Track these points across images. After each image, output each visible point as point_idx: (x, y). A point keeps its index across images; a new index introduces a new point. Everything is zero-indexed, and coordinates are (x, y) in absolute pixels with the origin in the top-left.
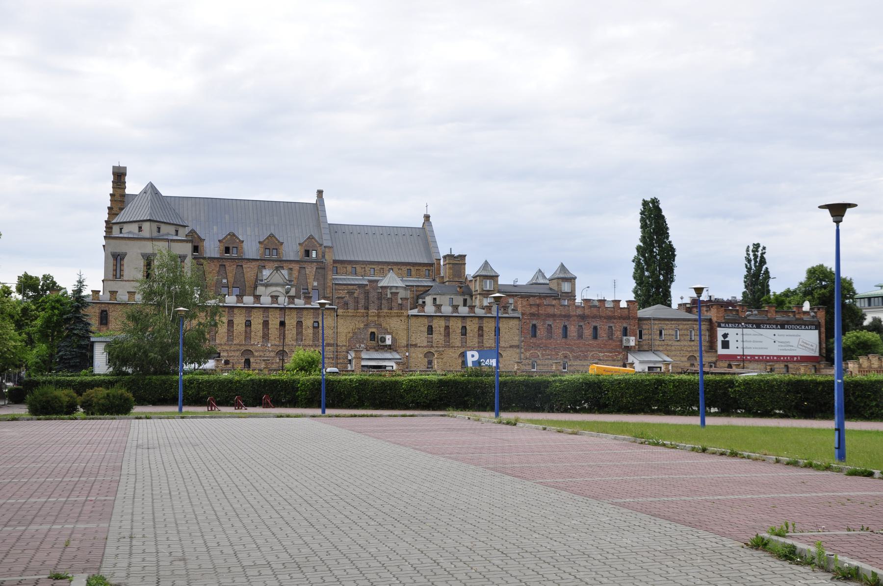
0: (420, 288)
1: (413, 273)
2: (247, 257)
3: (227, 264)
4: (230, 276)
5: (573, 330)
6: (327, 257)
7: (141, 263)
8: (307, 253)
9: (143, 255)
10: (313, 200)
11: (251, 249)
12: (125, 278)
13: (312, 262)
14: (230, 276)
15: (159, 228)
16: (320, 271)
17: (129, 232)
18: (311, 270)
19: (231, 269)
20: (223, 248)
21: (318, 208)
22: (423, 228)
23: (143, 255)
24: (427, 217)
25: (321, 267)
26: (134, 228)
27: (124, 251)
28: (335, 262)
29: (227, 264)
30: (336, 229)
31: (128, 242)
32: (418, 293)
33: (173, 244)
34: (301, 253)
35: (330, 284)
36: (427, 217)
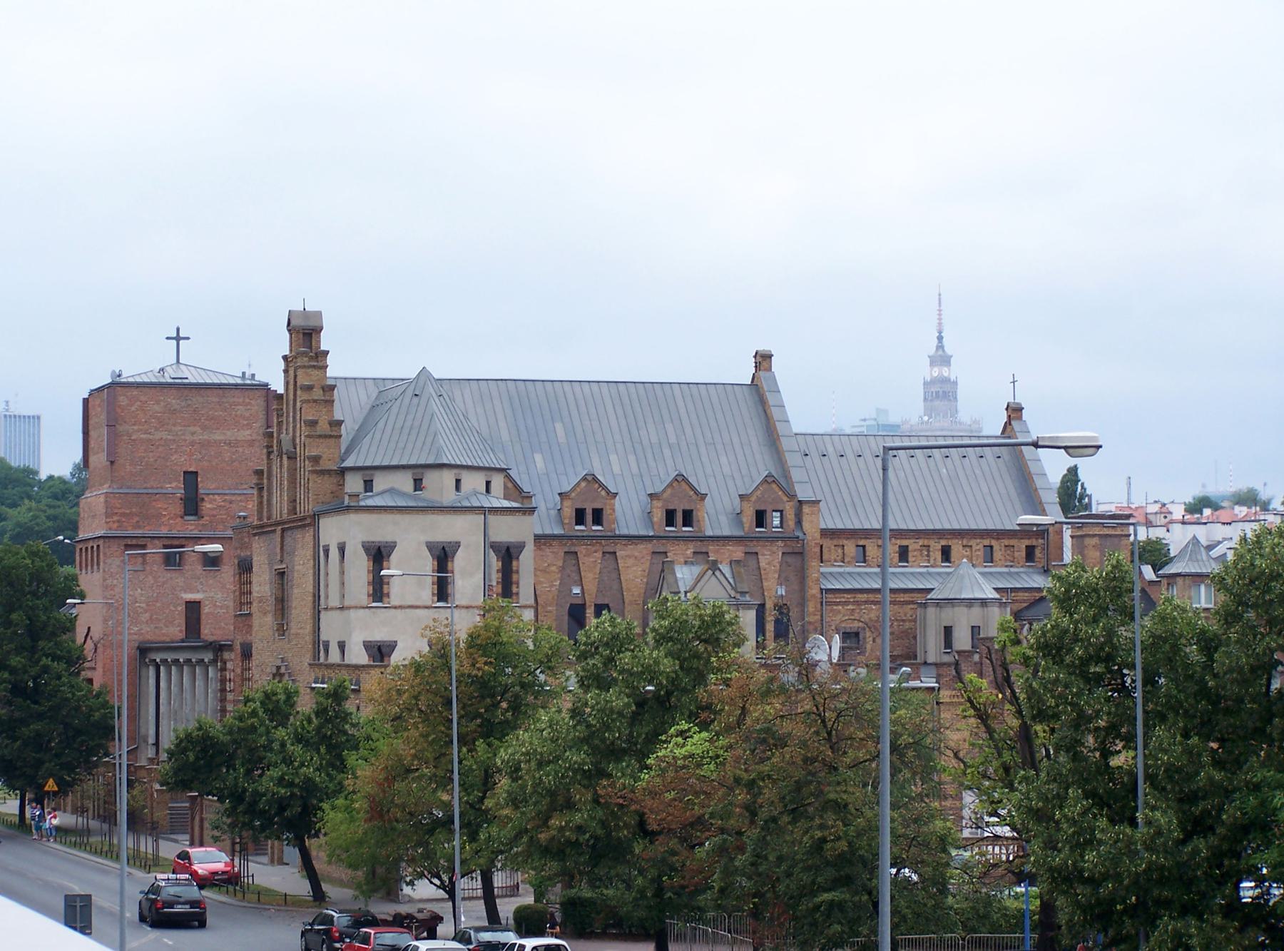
0: (1021, 595)
1: (998, 554)
2: (624, 532)
3: (581, 550)
4: (590, 578)
5: (872, 551)
6: (806, 525)
7: (428, 564)
8: (760, 518)
9: (431, 546)
10: (744, 373)
11: (629, 514)
12: (394, 600)
13: (772, 539)
14: (590, 578)
15: (458, 481)
16: (790, 559)
17: (391, 491)
18: (770, 559)
19: (591, 561)
20: (569, 512)
21: (760, 391)
22: (754, 384)
23: (431, 546)
24: (763, 360)
25: (796, 552)
26: (404, 482)
27: (389, 539)
28: (826, 533)
29: (581, 550)
30: (821, 447)
31: (398, 517)
32: (1017, 607)
33: (492, 519)
34: (749, 518)
35: (814, 591)
36: (763, 360)
